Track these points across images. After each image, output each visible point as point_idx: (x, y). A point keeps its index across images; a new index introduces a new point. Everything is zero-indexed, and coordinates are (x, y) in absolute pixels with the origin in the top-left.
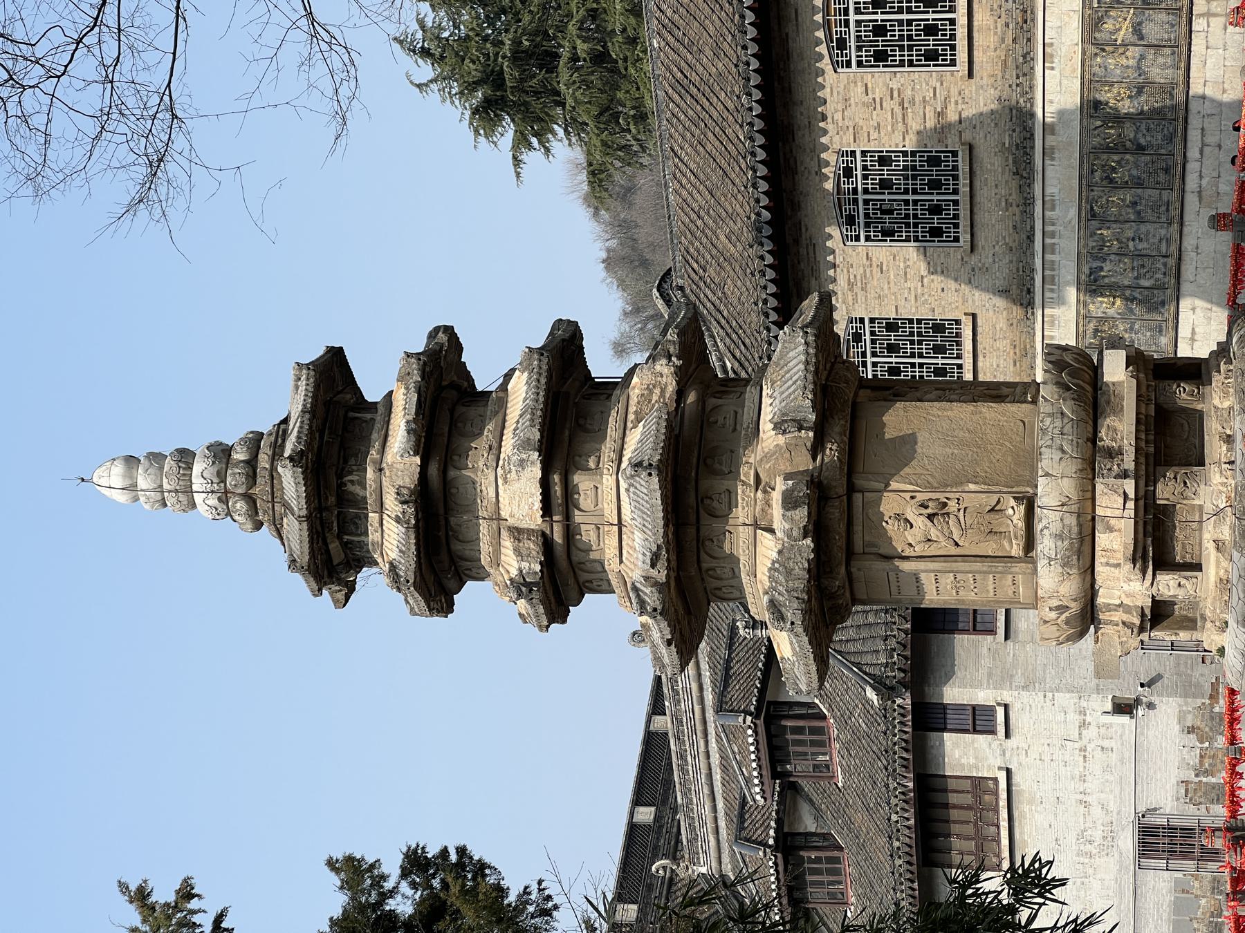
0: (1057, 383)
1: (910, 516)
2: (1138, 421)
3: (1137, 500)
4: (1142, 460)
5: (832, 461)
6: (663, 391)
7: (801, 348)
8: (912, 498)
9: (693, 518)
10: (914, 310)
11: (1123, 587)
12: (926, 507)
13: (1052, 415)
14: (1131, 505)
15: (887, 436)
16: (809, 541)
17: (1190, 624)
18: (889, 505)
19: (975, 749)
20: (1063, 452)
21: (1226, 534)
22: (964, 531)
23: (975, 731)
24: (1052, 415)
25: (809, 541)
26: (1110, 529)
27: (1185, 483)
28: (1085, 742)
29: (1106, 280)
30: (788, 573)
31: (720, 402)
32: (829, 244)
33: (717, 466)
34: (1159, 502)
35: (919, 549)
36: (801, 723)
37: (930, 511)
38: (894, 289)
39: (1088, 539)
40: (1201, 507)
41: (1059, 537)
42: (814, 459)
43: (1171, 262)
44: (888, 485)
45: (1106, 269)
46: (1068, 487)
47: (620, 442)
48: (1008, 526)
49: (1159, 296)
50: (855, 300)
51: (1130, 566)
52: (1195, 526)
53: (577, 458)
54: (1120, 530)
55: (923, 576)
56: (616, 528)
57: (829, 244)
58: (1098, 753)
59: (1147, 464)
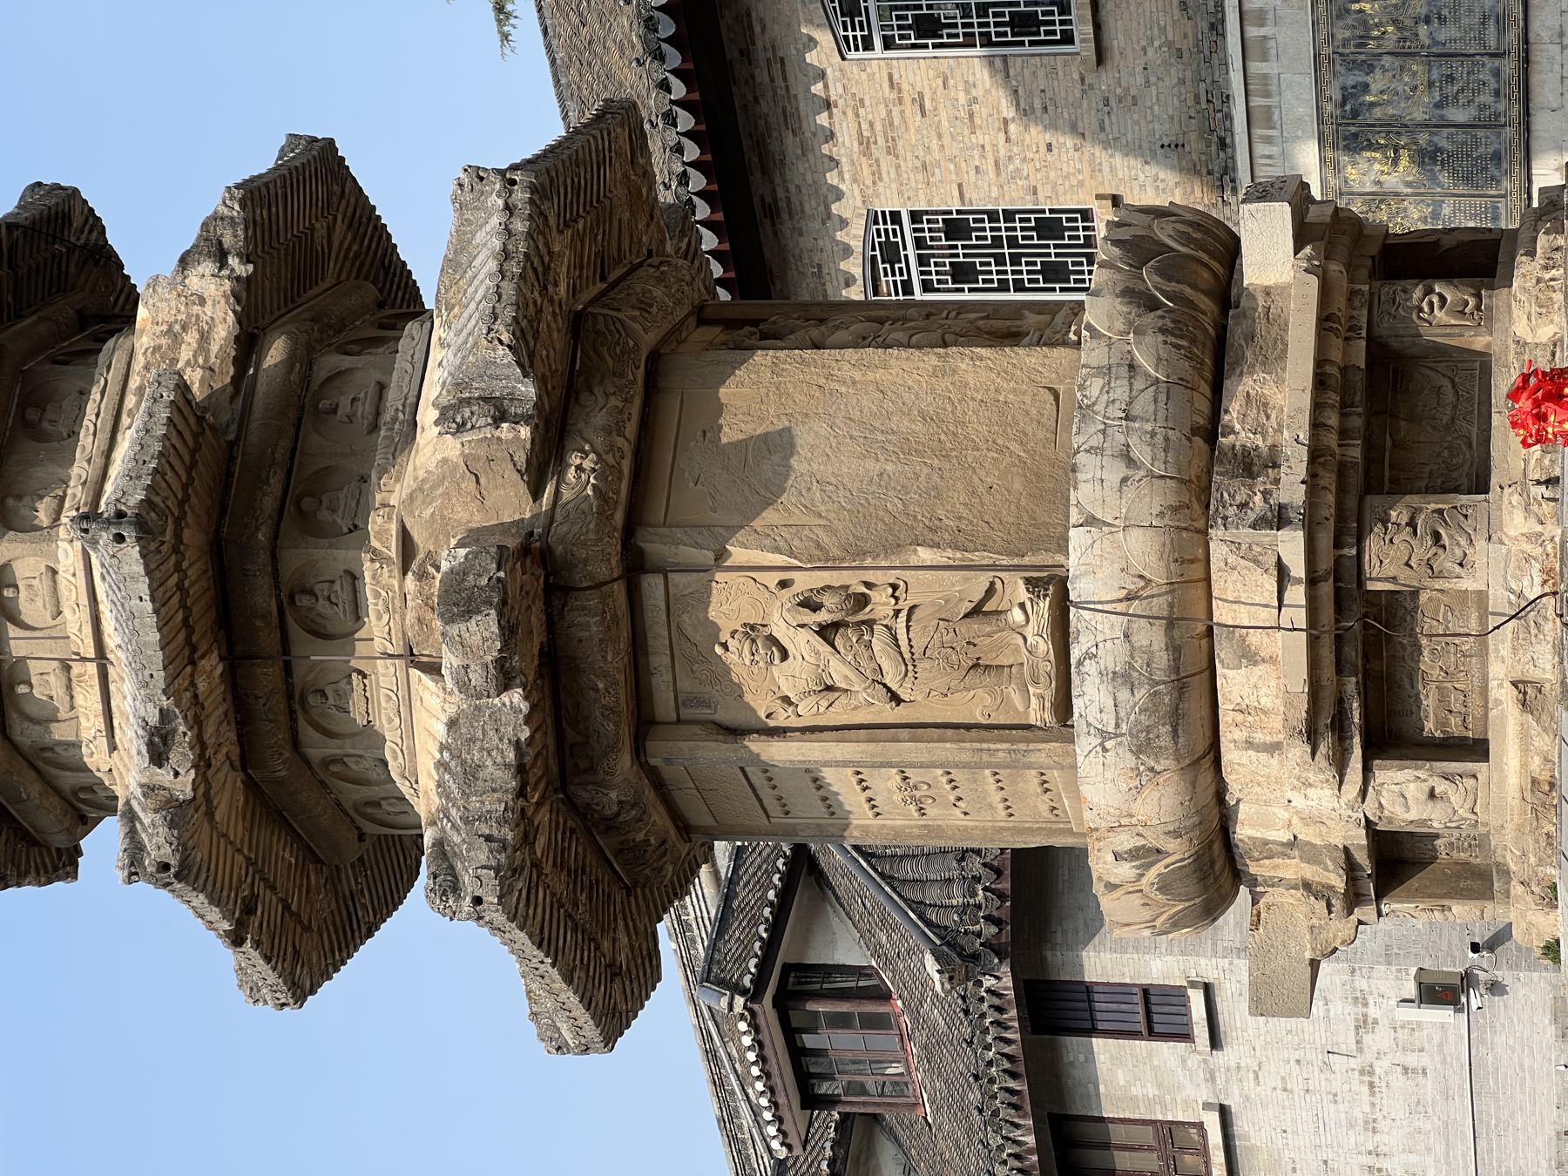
0: (1129, 294)
1: (780, 631)
2: (1320, 382)
3: (1312, 581)
4: (1328, 479)
5: (581, 498)
6: (204, 338)
7: (495, 221)
8: (784, 584)
9: (268, 640)
10: (995, 192)
11: (1295, 802)
12: (816, 608)
13: (1110, 344)
14: (1297, 594)
15: (728, 436)
16: (516, 697)
17: (1477, 884)
18: (732, 601)
19: (1153, 1068)
20: (1130, 462)
21: (1544, 667)
22: (909, 664)
23: (1152, 1034)
24: (1106, 371)
25: (516, 697)
26: (1249, 657)
27: (1437, 537)
28: (1369, 1056)
29: (1377, 112)
30: (470, 774)
31: (347, 362)
32: (811, 57)
33: (324, 515)
34: (1372, 586)
35: (809, 711)
36: (844, 1007)
37: (823, 617)
38: (952, 149)
39: (1198, 684)
40: (1482, 597)
41: (1122, 678)
42: (536, 494)
43: (1509, 66)
44: (721, 555)
45: (1374, 88)
46: (1143, 550)
47: (98, 461)
48: (1017, 650)
49: (1488, 142)
50: (877, 176)
51: (1300, 750)
52: (1468, 645)
53: (10, 502)
54: (1273, 660)
55: (828, 775)
56: (92, 668)
57: (811, 57)
58: (1398, 1079)
59: (1341, 490)
